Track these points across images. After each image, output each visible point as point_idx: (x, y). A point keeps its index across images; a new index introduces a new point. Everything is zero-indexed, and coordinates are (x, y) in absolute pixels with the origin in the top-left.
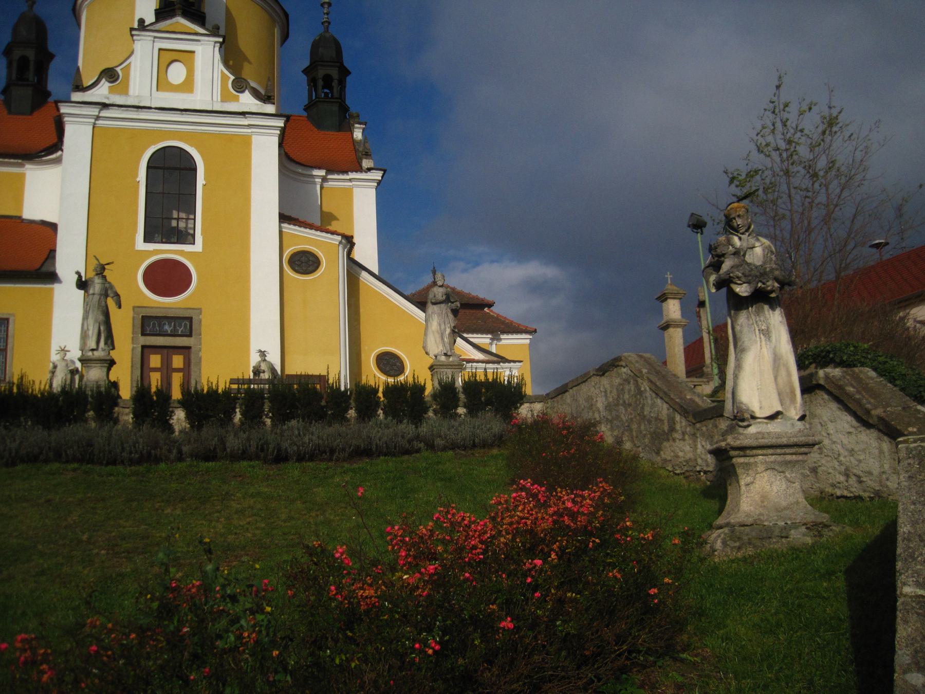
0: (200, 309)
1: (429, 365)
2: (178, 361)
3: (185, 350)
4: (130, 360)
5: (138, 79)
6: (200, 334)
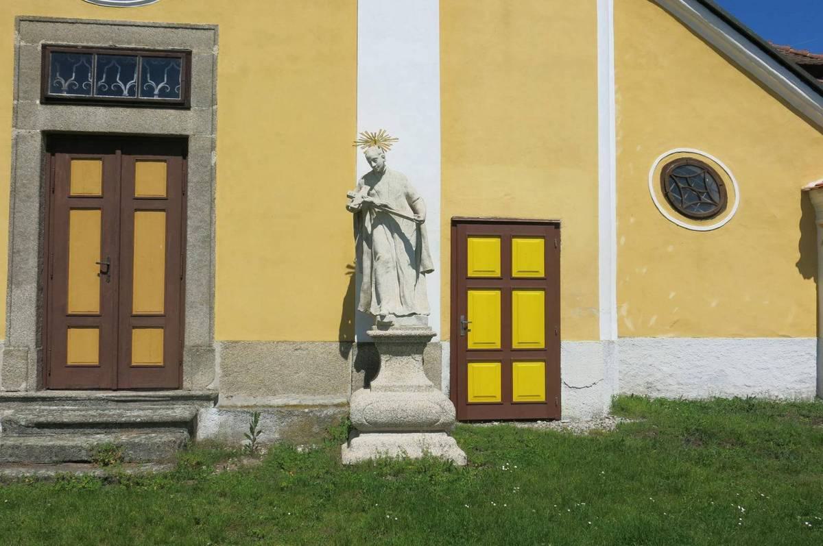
0: (213, 29)
1: (562, 225)
2: (83, 347)
3: (173, 147)
4: (7, 173)
5: (50, 71)
6: (213, 102)
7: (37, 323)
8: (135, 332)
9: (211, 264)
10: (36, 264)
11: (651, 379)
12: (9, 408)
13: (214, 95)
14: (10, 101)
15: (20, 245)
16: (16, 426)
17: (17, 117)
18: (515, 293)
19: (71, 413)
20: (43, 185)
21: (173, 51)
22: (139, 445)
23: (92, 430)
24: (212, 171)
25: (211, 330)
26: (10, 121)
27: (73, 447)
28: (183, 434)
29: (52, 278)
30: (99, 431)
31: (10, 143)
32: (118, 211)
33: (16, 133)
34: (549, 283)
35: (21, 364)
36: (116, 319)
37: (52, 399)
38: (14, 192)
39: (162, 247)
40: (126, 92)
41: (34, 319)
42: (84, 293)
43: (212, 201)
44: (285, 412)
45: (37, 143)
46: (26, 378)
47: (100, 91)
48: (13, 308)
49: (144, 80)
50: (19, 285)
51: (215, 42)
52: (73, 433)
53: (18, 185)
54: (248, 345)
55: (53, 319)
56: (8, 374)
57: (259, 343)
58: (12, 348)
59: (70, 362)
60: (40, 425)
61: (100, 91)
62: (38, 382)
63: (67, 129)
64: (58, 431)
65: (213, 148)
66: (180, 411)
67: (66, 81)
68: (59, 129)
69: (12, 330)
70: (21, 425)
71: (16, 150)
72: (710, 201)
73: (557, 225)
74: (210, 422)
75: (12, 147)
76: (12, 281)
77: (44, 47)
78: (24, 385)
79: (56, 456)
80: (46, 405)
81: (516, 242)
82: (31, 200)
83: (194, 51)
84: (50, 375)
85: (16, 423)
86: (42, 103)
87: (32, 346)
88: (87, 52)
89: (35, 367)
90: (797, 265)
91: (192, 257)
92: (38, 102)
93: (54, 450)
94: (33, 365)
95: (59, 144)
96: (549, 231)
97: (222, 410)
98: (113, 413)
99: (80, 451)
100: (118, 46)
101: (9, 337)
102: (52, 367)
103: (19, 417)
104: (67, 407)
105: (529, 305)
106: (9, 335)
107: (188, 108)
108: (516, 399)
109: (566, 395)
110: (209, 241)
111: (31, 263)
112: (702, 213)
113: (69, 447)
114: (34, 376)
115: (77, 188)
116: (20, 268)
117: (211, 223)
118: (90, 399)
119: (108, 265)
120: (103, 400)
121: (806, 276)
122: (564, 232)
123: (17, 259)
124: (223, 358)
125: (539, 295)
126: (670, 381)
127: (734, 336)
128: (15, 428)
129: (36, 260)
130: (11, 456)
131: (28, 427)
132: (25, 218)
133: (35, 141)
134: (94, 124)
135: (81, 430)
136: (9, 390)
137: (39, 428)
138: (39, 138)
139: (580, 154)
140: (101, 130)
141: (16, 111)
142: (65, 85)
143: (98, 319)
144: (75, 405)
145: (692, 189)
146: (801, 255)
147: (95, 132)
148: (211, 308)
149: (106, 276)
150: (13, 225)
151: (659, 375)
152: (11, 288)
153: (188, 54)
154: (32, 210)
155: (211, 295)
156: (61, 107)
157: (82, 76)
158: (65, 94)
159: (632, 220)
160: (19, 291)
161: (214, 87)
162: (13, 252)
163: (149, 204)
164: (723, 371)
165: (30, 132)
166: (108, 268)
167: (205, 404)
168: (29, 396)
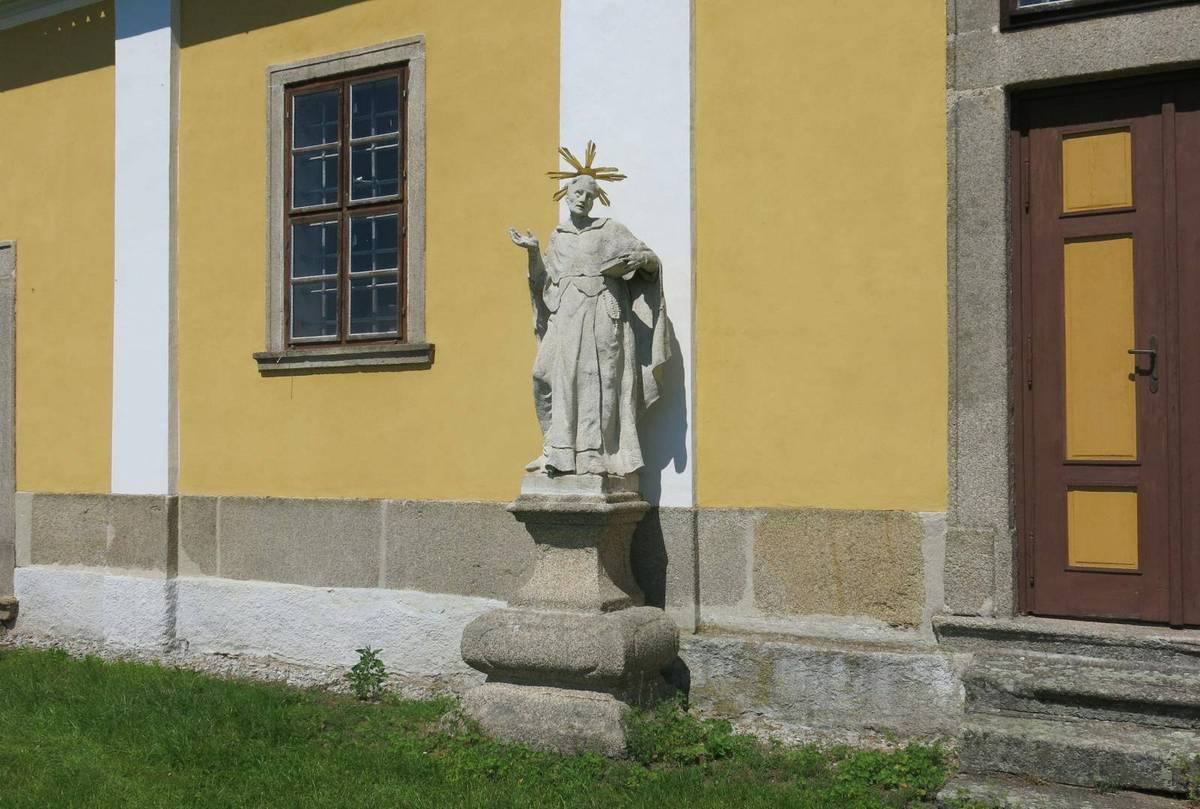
10: (1004, 360)
12: (962, 649)
14: (940, 38)
16: (994, 692)
17: (955, 67)
19: (1102, 676)
20: (1010, 199)
23: (1161, 718)
27: (1141, 758)
29: (1030, 387)
30: (1177, 722)
31: (944, 120)
33: (954, 99)
37: (1049, 639)
38: (955, 217)
45: (997, 112)
46: (992, 591)
48: (960, 449)
50: (971, 400)
52: (1117, 720)
53: (962, 202)
55: (1041, 474)
56: (955, 579)
58: (963, 529)
60: (1047, 697)
63: (1058, 75)
64: (1084, 711)
67: (395, 303)
68: (1041, 77)
69: (960, 493)
70: (1005, 690)
71: (957, 134)
75: (949, 128)
76: (959, 395)
78: (988, 604)
79: (1102, 773)
80: (1037, 650)
82: (990, 229)
84: (1032, 585)
85: (995, 686)
86: (1003, 30)
87: (1002, 524)
89: (1010, 569)
92: (996, 29)
93: (1098, 759)
94: (1004, 565)
95: (1038, 108)
99: (1158, 768)
101: (956, 506)
102: (1041, 573)
103: (997, 674)
104: (1084, 659)
106: (954, 504)
111: (994, 357)
113: (1131, 756)
114: (1008, 587)
115: (1078, 195)
116: (974, 368)
118: (1132, 645)
119: (1153, 356)
120: (1163, 648)
123: (966, 350)
125: (1079, 447)
128: (993, 697)
129: (1004, 349)
130: (1004, 759)
131: (1021, 696)
132: (978, 267)
133: (993, 109)
134: (1118, 53)
135: (1137, 716)
136: (958, 611)
137: (1043, 701)
140: (1133, 64)
141: (952, 55)
143: (1133, 472)
144: (1100, 655)
147: (1120, 71)
149: (1147, 378)
150: (955, 282)
152: (957, 408)
154: (992, 249)
156: (1043, 30)
160: (972, 415)
162: (959, 337)
165: (981, 93)
166: (1153, 363)
168: (1003, 628)
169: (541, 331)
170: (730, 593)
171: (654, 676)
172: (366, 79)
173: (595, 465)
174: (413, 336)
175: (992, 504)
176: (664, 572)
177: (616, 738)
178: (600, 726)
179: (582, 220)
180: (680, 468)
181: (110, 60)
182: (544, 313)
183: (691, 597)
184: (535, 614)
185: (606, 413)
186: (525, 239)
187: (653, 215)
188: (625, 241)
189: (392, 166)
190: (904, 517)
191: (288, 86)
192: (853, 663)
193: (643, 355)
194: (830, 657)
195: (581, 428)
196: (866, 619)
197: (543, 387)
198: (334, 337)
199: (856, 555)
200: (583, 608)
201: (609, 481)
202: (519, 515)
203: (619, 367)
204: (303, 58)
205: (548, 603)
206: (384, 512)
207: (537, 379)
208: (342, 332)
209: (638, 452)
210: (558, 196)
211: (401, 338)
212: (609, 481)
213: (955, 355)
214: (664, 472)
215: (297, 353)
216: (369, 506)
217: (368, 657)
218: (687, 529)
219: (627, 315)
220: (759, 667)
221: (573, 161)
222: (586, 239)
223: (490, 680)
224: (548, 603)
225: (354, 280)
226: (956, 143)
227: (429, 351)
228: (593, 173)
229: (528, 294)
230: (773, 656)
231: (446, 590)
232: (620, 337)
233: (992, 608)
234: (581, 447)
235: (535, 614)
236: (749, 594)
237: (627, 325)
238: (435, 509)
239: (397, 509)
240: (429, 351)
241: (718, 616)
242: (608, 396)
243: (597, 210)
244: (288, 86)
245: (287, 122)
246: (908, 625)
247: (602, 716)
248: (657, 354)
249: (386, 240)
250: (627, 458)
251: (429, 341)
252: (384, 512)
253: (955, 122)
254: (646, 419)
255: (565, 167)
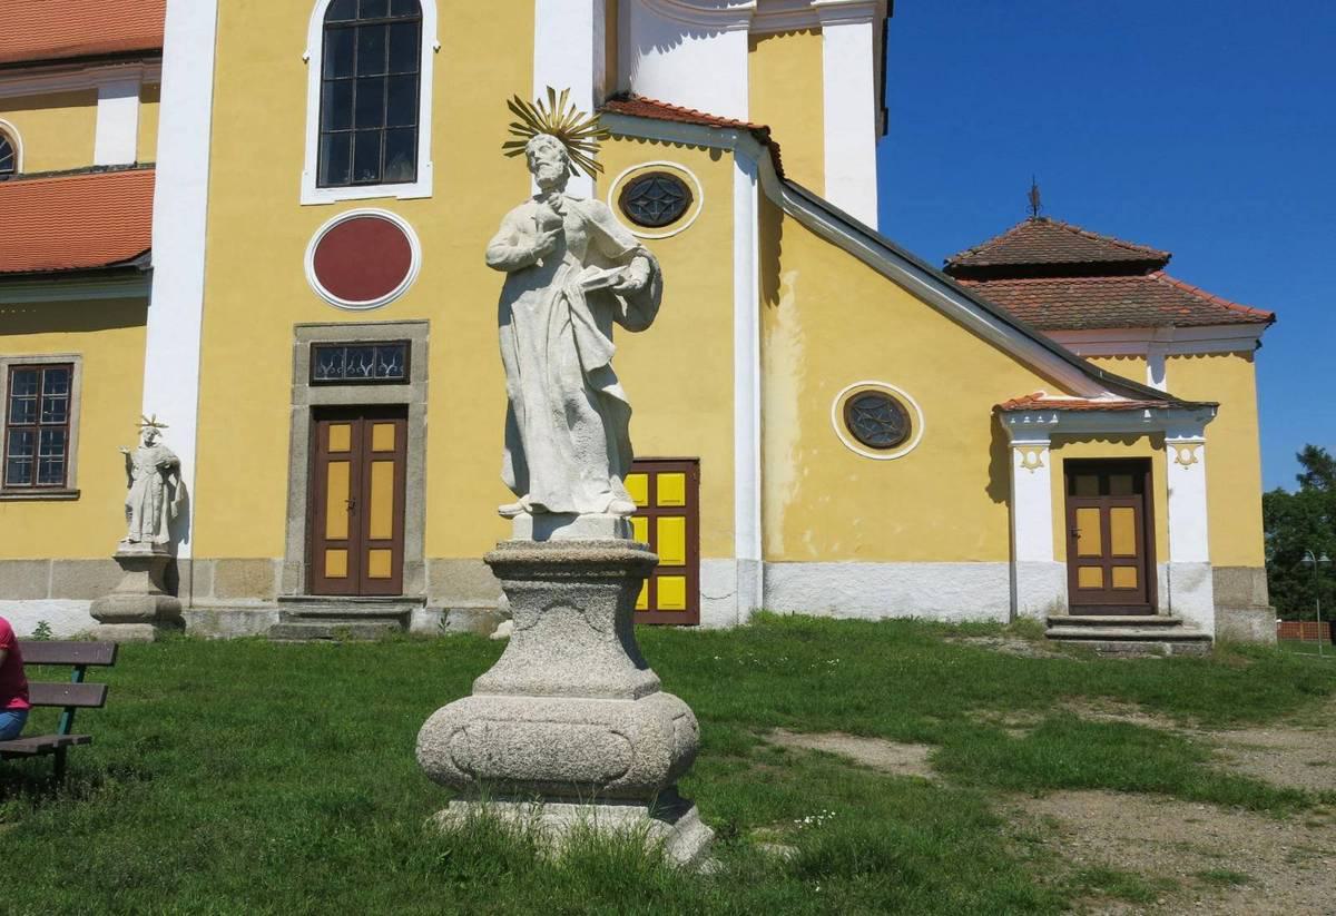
1: (701, 462)
2: (336, 563)
3: (396, 413)
6: (426, 377)
7: (306, 545)
8: (372, 552)
9: (423, 500)
11: (833, 602)
13: (426, 372)
15: (295, 490)
18: (659, 519)
21: (398, 341)
22: (363, 627)
24: (425, 431)
25: (422, 551)
26: (289, 401)
28: (397, 623)
32: (361, 460)
34: (690, 511)
35: (294, 574)
36: (359, 543)
38: (291, 451)
39: (391, 487)
40: (366, 374)
41: (303, 542)
42: (337, 524)
43: (425, 451)
44: (472, 612)
45: (306, 415)
46: (298, 585)
47: (349, 374)
49: (379, 364)
51: (427, 332)
54: (448, 562)
55: (316, 543)
57: (456, 559)
59: (327, 575)
61: (349, 374)
62: (305, 589)
65: (425, 413)
66: (398, 609)
72: (1109, 398)
73: (696, 462)
74: (421, 619)
77: (312, 344)
78: (295, 591)
81: (661, 477)
83: (413, 340)
87: (302, 561)
88: (339, 347)
90: (987, 489)
91: (410, 494)
96: (690, 467)
97: (430, 610)
98: (353, 609)
100: (362, 340)
105: (1090, 544)
106: (287, 554)
107: (409, 383)
108: (660, 607)
109: (703, 604)
110: (422, 482)
112: (882, 442)
117: (424, 469)
121: (997, 500)
122: (703, 467)
124: (431, 572)
126: (854, 604)
127: (919, 561)
138: (308, 411)
139: (720, 402)
141: (293, 393)
142: (326, 372)
145: (877, 420)
146: (992, 481)
148: (423, 533)
150: (290, 474)
151: (842, 599)
153: (409, 342)
154: (303, 463)
155: (423, 524)
157: (338, 364)
158: (326, 379)
159: (815, 452)
161: (427, 366)
162: (291, 493)
163: (382, 456)
164: (908, 594)
167: (417, 605)
169: (130, 486)
170: (205, 592)
171: (168, 619)
172: (53, 368)
173: (150, 539)
174: (70, 486)
175: (299, 554)
176: (177, 584)
177: (151, 637)
178: (146, 635)
179: (149, 444)
180: (186, 542)
181: (96, 104)
182: (131, 480)
183: (188, 594)
184: (121, 597)
185: (155, 520)
186: (125, 450)
187: (179, 442)
188: (166, 453)
189: (62, 409)
190: (269, 560)
191: (9, 366)
192: (248, 614)
193: (171, 497)
194: (239, 613)
195: (144, 525)
196: (254, 599)
197: (129, 509)
198: (29, 484)
199: (247, 574)
200: (142, 593)
201: (154, 545)
202: (117, 559)
203: (161, 502)
204: (21, 354)
205: (127, 592)
206: (52, 564)
207: (127, 506)
208: (34, 483)
209: (167, 534)
210: (140, 432)
211: (64, 486)
212: (154, 545)
213: (289, 500)
214: (180, 545)
215: (9, 491)
216: (44, 562)
217: (43, 625)
218: (188, 567)
219: (166, 481)
220: (213, 617)
221: (146, 420)
222: (150, 451)
223: (102, 623)
224: (127, 592)
225: (41, 459)
226: (293, 425)
227: (78, 493)
228: (154, 425)
229: (125, 471)
230: (218, 614)
231: (81, 598)
232: (162, 490)
233: (297, 591)
234: (144, 532)
235: (121, 597)
236: (212, 592)
237: (165, 487)
238: (77, 563)
239: (58, 563)
240: (78, 493)
241: (200, 601)
242: (156, 513)
243: (156, 439)
244: (9, 366)
245: (9, 383)
246: (269, 600)
247: (146, 631)
248: (177, 498)
249: (58, 440)
250: (163, 537)
251: (78, 488)
252: (52, 564)
253: (293, 417)
254: (172, 523)
255: (144, 422)
